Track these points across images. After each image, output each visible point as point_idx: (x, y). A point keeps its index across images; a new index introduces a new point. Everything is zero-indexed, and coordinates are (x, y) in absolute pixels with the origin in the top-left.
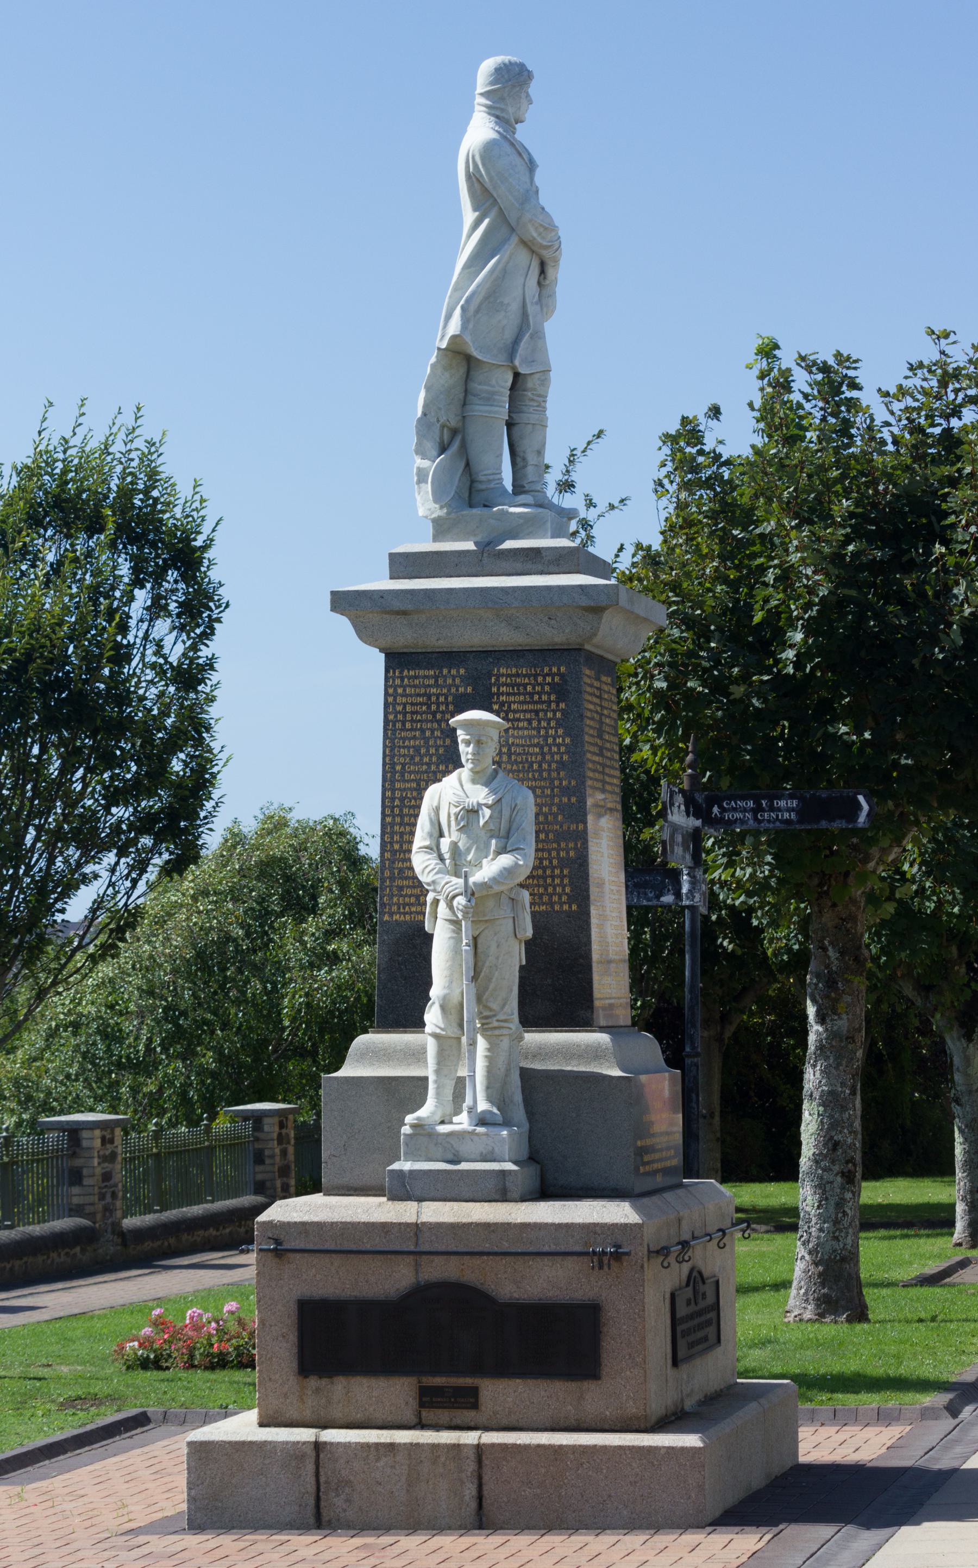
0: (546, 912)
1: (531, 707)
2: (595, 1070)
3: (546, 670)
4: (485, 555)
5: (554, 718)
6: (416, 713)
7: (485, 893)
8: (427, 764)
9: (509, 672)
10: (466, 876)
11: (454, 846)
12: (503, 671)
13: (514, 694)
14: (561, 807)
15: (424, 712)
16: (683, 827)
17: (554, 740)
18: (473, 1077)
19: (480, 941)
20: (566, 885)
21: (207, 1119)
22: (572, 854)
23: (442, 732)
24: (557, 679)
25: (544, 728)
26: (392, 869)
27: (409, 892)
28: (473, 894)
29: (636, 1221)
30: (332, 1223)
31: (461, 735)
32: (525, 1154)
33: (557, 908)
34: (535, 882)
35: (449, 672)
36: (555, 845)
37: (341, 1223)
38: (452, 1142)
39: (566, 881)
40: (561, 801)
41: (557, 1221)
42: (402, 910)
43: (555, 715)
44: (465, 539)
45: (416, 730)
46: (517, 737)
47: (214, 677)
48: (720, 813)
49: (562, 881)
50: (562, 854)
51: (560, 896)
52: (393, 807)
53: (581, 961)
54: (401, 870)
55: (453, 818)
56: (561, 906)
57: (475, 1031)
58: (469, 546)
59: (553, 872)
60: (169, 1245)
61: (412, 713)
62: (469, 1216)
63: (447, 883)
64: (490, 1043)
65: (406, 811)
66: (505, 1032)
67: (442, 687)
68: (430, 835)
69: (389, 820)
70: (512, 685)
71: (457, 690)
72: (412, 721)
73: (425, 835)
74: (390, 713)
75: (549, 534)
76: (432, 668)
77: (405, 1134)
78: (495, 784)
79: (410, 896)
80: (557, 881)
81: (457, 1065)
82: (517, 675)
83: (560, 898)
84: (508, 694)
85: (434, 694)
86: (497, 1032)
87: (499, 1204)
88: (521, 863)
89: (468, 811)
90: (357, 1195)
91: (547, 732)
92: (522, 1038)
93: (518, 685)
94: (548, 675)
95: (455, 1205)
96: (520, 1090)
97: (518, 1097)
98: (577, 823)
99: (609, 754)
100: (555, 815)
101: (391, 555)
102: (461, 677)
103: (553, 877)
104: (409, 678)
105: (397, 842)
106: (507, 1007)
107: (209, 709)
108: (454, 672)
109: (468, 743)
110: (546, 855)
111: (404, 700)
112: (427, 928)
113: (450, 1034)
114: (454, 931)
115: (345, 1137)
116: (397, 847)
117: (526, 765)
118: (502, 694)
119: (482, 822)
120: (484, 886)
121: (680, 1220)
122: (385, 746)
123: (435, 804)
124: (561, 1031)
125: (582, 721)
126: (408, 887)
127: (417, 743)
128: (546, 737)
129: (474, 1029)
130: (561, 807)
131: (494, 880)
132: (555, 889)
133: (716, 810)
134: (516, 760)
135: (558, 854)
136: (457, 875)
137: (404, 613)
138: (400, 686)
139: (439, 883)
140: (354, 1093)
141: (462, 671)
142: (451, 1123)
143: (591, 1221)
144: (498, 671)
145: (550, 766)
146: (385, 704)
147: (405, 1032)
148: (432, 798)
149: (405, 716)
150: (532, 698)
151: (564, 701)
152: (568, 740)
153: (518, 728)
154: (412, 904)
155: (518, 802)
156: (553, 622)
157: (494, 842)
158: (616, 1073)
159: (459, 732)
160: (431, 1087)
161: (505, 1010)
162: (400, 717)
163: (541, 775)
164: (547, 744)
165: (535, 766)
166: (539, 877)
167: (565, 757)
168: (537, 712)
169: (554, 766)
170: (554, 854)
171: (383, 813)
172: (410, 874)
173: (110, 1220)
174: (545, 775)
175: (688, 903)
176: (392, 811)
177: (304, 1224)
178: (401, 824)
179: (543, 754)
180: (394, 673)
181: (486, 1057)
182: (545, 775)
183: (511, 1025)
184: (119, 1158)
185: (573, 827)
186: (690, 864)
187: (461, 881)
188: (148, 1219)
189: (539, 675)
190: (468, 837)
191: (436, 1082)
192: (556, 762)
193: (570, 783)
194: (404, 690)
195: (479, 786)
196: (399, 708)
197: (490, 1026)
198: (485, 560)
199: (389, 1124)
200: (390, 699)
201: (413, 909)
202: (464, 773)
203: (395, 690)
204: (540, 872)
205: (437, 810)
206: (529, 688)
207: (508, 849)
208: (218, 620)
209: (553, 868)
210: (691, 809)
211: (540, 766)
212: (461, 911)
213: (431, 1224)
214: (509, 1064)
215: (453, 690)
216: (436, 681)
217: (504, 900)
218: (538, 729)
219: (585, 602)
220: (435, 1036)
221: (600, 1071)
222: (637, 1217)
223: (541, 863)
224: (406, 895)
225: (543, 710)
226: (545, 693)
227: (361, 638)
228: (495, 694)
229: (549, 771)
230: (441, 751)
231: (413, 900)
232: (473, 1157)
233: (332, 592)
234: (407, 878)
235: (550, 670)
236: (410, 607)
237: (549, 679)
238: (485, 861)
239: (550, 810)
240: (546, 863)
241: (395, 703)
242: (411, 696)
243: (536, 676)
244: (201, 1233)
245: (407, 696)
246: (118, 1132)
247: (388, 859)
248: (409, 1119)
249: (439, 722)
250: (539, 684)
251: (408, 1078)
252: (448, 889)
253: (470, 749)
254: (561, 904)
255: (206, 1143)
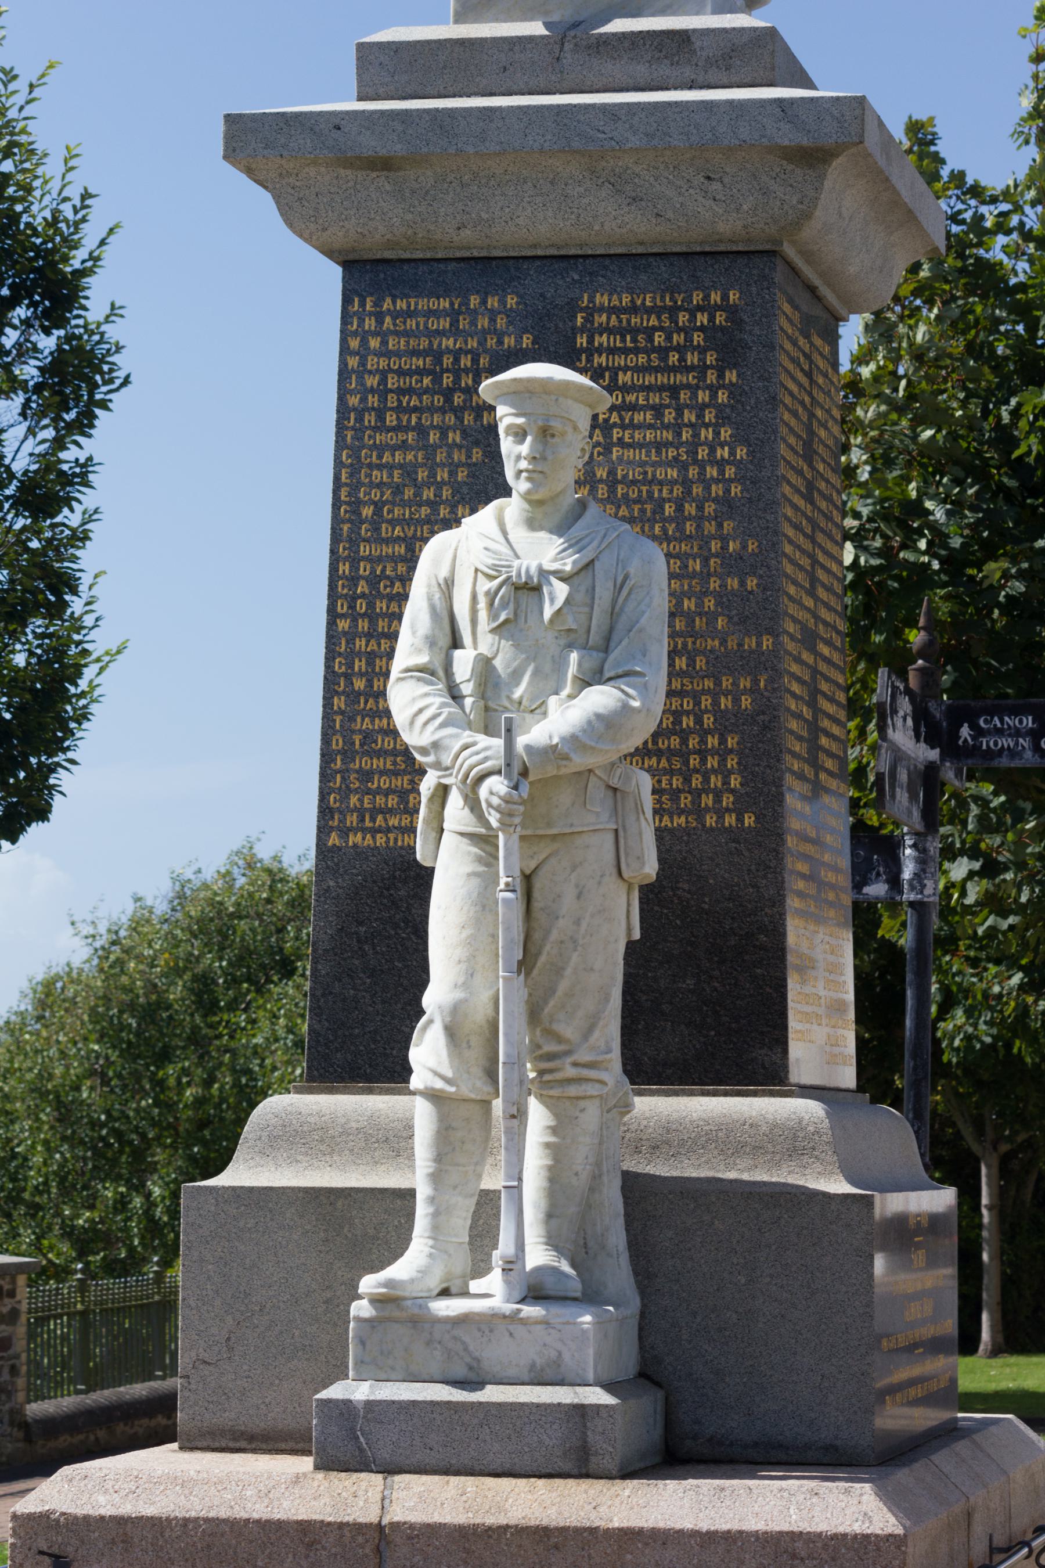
0: (687, 831)
1: (661, 379)
2: (790, 1180)
3: (697, 298)
4: (567, 46)
5: (713, 403)
6: (409, 391)
7: (551, 771)
8: (429, 503)
9: (615, 302)
10: (509, 730)
11: (485, 667)
12: (602, 299)
13: (625, 351)
14: (723, 597)
15: (426, 391)
16: (909, 758)
17: (712, 450)
18: (516, 1191)
19: (538, 884)
20: (730, 772)
21: (158, 1263)
22: (746, 702)
23: (465, 434)
24: (720, 318)
25: (691, 425)
26: (347, 733)
27: (384, 783)
28: (525, 773)
29: (889, 1530)
30: (186, 1521)
31: (506, 416)
32: (629, 1366)
33: (710, 821)
34: (664, 763)
35: (484, 302)
36: (709, 683)
37: (207, 1520)
38: (467, 1339)
39: (732, 762)
40: (723, 586)
41: (704, 1526)
42: (368, 824)
43: (714, 396)
44: (526, 16)
45: (407, 429)
46: (629, 446)
47: (88, 499)
48: (973, 738)
49: (723, 761)
50: (725, 703)
51: (718, 795)
52: (354, 598)
53: (762, 937)
54: (368, 737)
55: (482, 604)
56: (721, 817)
57: (524, 1089)
58: (536, 28)
59: (703, 741)
60: (97, 1439)
61: (401, 392)
62: (500, 1510)
63: (466, 747)
64: (556, 1115)
65: (381, 606)
66: (592, 1090)
67: (467, 335)
68: (431, 642)
69: (343, 625)
70: (622, 332)
71: (500, 342)
72: (399, 409)
73: (419, 641)
74: (351, 392)
75: (709, 8)
76: (446, 294)
77: (359, 1319)
78: (578, 530)
79: (387, 793)
80: (712, 762)
81: (480, 1163)
82: (633, 309)
83: (718, 799)
84: (612, 351)
85: (449, 351)
86: (573, 1090)
87: (571, 1482)
88: (636, 704)
89: (517, 588)
90: (254, 1451)
91: (696, 435)
92: (628, 1107)
93: (635, 331)
94: (700, 308)
95: (469, 1483)
96: (621, 1220)
97: (617, 1238)
98: (759, 636)
99: (823, 505)
100: (711, 618)
101: (361, 46)
102: (508, 313)
103: (703, 753)
104: (395, 315)
105: (361, 674)
106: (597, 1034)
107: (78, 553)
108: (493, 302)
109: (520, 434)
110: (687, 704)
111: (383, 363)
112: (421, 855)
113: (466, 1092)
114: (479, 860)
115: (229, 1319)
116: (359, 684)
117: (648, 507)
118: (599, 351)
119: (548, 612)
120: (550, 753)
121: (969, 1515)
122: (338, 463)
123: (444, 573)
124: (715, 1094)
125: (774, 410)
126: (382, 773)
127: (410, 457)
128: (694, 444)
129: (521, 1082)
130: (723, 597)
131: (573, 740)
132: (706, 780)
133: (965, 732)
134: (625, 496)
135: (716, 703)
136: (488, 730)
137: (385, 164)
138: (375, 334)
139: (447, 748)
140: (251, 1223)
141: (511, 301)
142: (465, 1293)
143: (785, 1527)
144: (591, 300)
145: (700, 508)
146: (341, 373)
147: (370, 1091)
148: (436, 562)
149: (384, 399)
150: (664, 359)
151: (735, 366)
152: (741, 453)
153: (632, 426)
154: (391, 811)
155: (632, 571)
156: (716, 186)
157: (574, 656)
158: (839, 1186)
159: (501, 410)
160: (422, 1211)
161: (592, 1039)
162: (373, 400)
163: (679, 528)
164: (695, 461)
165: (669, 510)
166: (671, 753)
167: (735, 490)
168: (674, 391)
169: (710, 508)
170: (706, 702)
171: (331, 611)
172: (388, 744)
173: (7, 1407)
174: (689, 527)
175: (912, 897)
176: (352, 607)
177: (121, 1521)
178: (369, 636)
179: (686, 483)
180: (363, 304)
181: (548, 1145)
182: (689, 527)
183: (604, 1076)
184: (23, 1318)
185: (750, 643)
186: (919, 827)
187: (498, 743)
188: (65, 1403)
189: (681, 308)
190: (516, 646)
191: (431, 1200)
192: (716, 500)
193: (744, 547)
194: (384, 343)
195: (543, 535)
196: (372, 381)
197: (558, 1076)
198: (568, 58)
199: (328, 1294)
200: (353, 362)
201: (393, 821)
202: (512, 507)
203: (364, 342)
204: (675, 742)
205: (448, 586)
206: (659, 338)
207: (607, 675)
208: (104, 405)
209: (704, 733)
210: (923, 729)
211: (680, 509)
212: (497, 809)
213: (412, 1526)
214: (598, 1164)
215: (491, 342)
216: (455, 323)
217: (596, 790)
218: (677, 428)
219: (787, 137)
220: (433, 1096)
221: (801, 1183)
222: (892, 1520)
223: (677, 721)
224: (378, 791)
225: (688, 386)
226: (695, 348)
227: (290, 224)
228: (582, 350)
229: (700, 519)
230: (462, 475)
231: (392, 801)
232: (512, 1372)
233: (228, 118)
234: (381, 753)
235: (707, 297)
236: (399, 149)
237: (702, 319)
238: (553, 700)
239: (700, 605)
240: (687, 722)
241: (363, 371)
242: (398, 354)
243: (673, 311)
244: (145, 1422)
245: (388, 354)
246: (22, 1280)
247: (342, 712)
248: (368, 1283)
249: (458, 412)
250: (679, 330)
251: (373, 1191)
252: (468, 759)
253: (525, 449)
254: (720, 813)
255: (157, 1298)
